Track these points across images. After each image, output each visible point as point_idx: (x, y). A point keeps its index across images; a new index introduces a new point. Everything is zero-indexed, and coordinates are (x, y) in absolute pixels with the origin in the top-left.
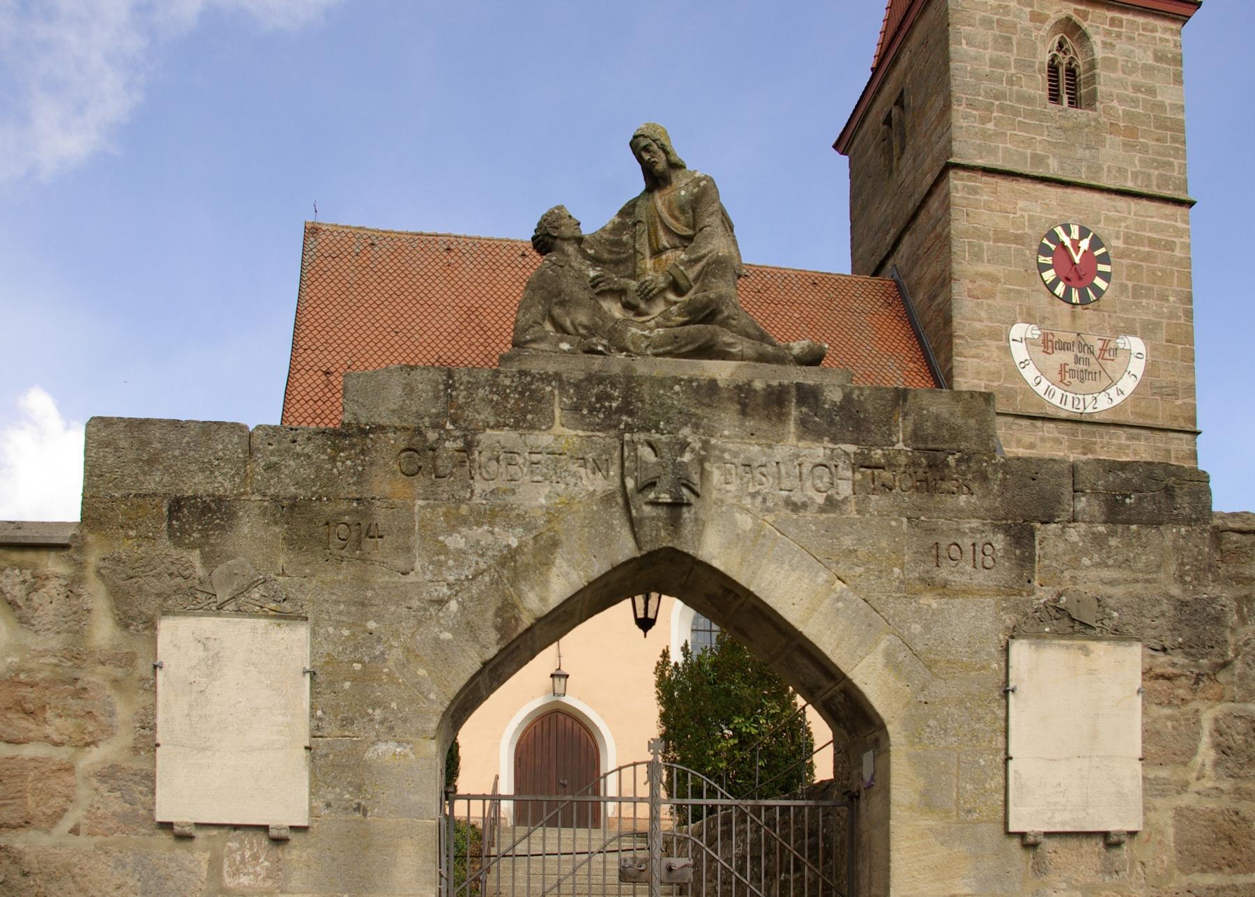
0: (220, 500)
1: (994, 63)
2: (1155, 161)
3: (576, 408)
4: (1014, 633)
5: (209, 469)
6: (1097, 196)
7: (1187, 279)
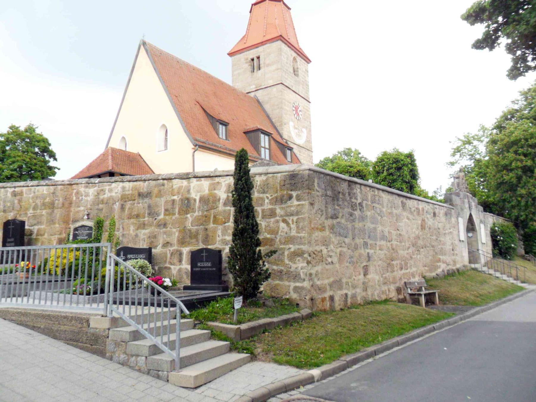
6: (299, 97)
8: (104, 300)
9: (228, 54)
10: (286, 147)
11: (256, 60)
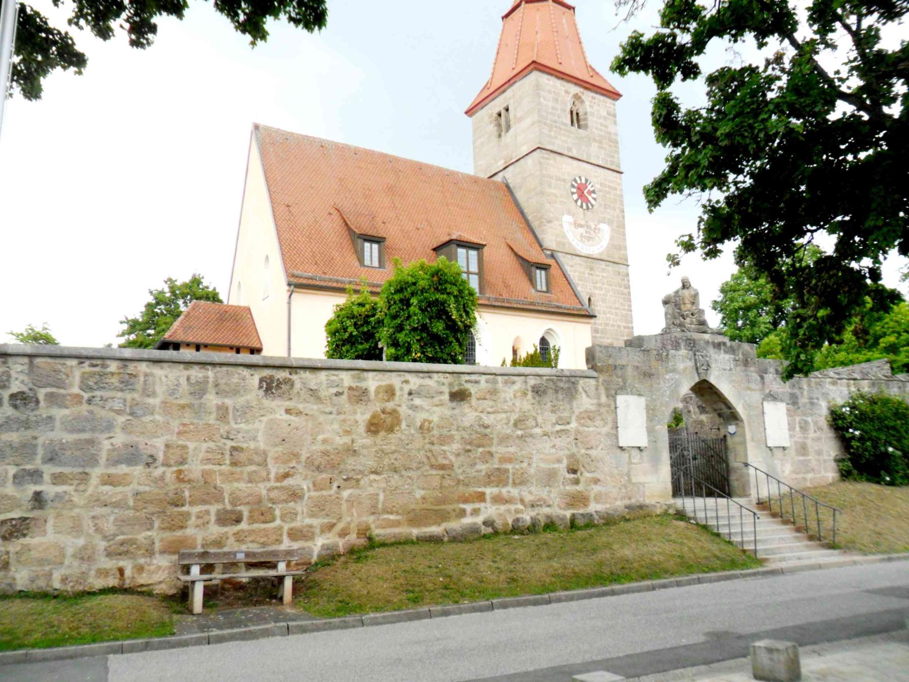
1: (553, 108)
4: (763, 400)
7: (622, 203)
8: (688, 493)
9: (466, 113)
10: (532, 266)
11: (503, 113)
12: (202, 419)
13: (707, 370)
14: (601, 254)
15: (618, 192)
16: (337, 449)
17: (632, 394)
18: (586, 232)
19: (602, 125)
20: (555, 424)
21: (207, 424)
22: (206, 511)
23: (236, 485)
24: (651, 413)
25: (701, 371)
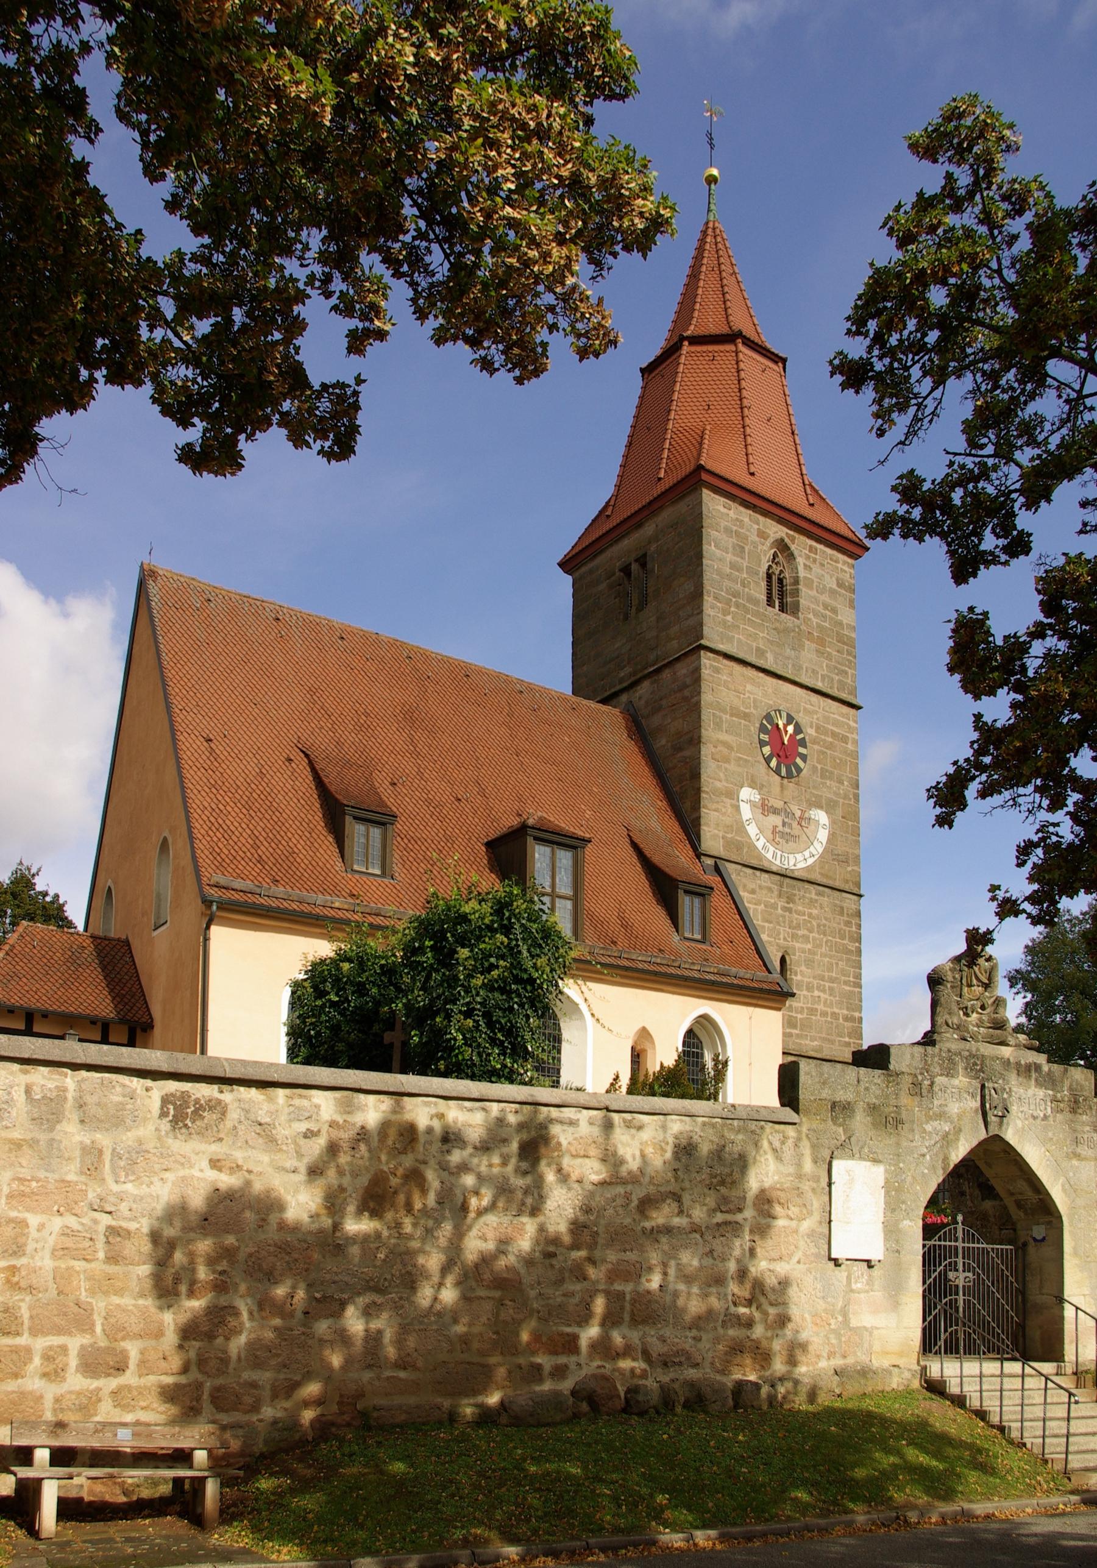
0: (849, 1103)
2: (836, 668)
3: (966, 1069)
5: (844, 1088)
6: (799, 690)
8: (952, 1349)
12: (53, 1171)
13: (1003, 1116)
14: (808, 869)
15: (850, 746)
16: (305, 1241)
17: (861, 1158)
18: (784, 824)
19: (826, 607)
20: (714, 1211)
21: (63, 1181)
22: (60, 1347)
23: (116, 1300)
24: (894, 1195)
25: (992, 1119)
